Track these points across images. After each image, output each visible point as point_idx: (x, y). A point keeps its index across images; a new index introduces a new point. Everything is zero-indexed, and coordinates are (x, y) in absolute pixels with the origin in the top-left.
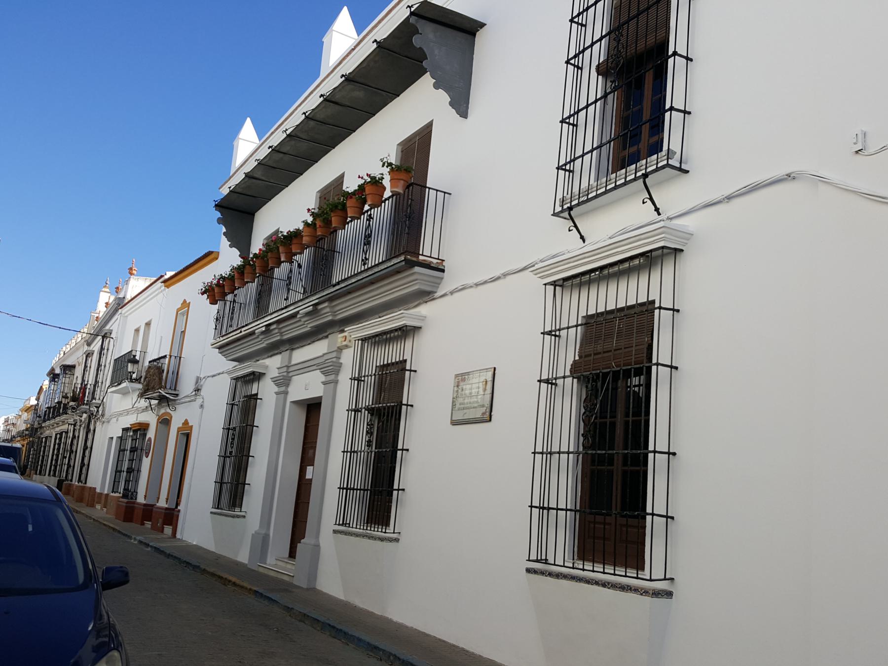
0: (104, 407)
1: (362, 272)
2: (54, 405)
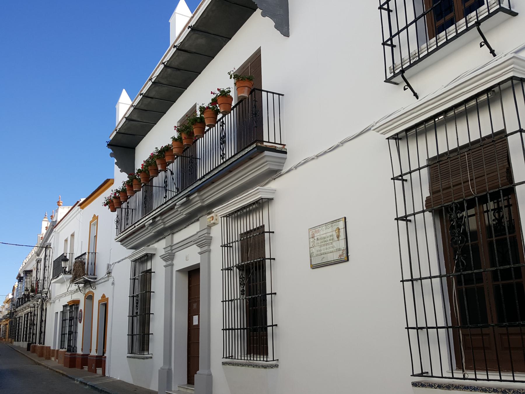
0: (50, 294)
1: (221, 164)
2: (22, 296)
